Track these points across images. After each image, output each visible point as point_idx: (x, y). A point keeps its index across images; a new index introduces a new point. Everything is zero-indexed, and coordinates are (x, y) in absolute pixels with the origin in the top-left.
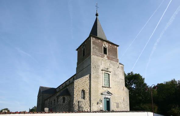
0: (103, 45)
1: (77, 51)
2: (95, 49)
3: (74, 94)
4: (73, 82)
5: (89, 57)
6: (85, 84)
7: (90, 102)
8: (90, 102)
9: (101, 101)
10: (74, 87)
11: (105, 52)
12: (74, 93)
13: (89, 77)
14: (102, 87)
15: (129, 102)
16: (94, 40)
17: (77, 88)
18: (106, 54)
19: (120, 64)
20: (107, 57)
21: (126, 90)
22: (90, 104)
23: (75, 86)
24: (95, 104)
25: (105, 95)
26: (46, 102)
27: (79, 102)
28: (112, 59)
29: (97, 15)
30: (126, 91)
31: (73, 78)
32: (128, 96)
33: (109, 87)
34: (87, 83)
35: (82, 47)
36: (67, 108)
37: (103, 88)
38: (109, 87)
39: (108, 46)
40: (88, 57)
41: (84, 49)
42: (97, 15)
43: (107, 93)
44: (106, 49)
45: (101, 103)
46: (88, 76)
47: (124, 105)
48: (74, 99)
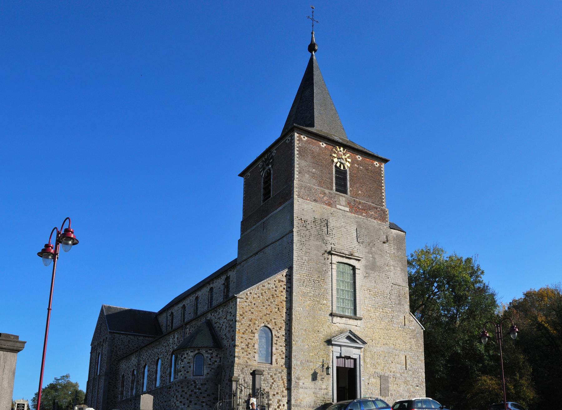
0: (336, 160)
1: (242, 180)
2: (307, 176)
3: (237, 343)
4: (229, 300)
5: (287, 203)
6: (273, 306)
7: (289, 374)
8: (289, 374)
9: (328, 368)
10: (235, 316)
11: (342, 187)
12: (234, 340)
13: (284, 279)
14: (331, 315)
15: (426, 373)
16: (307, 141)
17: (245, 322)
18: (345, 192)
19: (393, 226)
20: (349, 204)
21: (415, 326)
22: (289, 380)
23: (238, 314)
24: (307, 381)
25: (340, 346)
26: (123, 366)
27: (254, 374)
28: (365, 209)
29: (312, 48)
30: (413, 331)
31: (224, 277)
32: (421, 342)
33: (355, 316)
34: (278, 300)
35: (260, 164)
36: (208, 395)
37: (336, 319)
38: (355, 316)
39: (352, 163)
40: (281, 204)
41: (269, 174)
42: (312, 48)
43: (348, 338)
44: (345, 172)
45: (326, 377)
46: (282, 275)
47: (406, 382)
48: (233, 362)
